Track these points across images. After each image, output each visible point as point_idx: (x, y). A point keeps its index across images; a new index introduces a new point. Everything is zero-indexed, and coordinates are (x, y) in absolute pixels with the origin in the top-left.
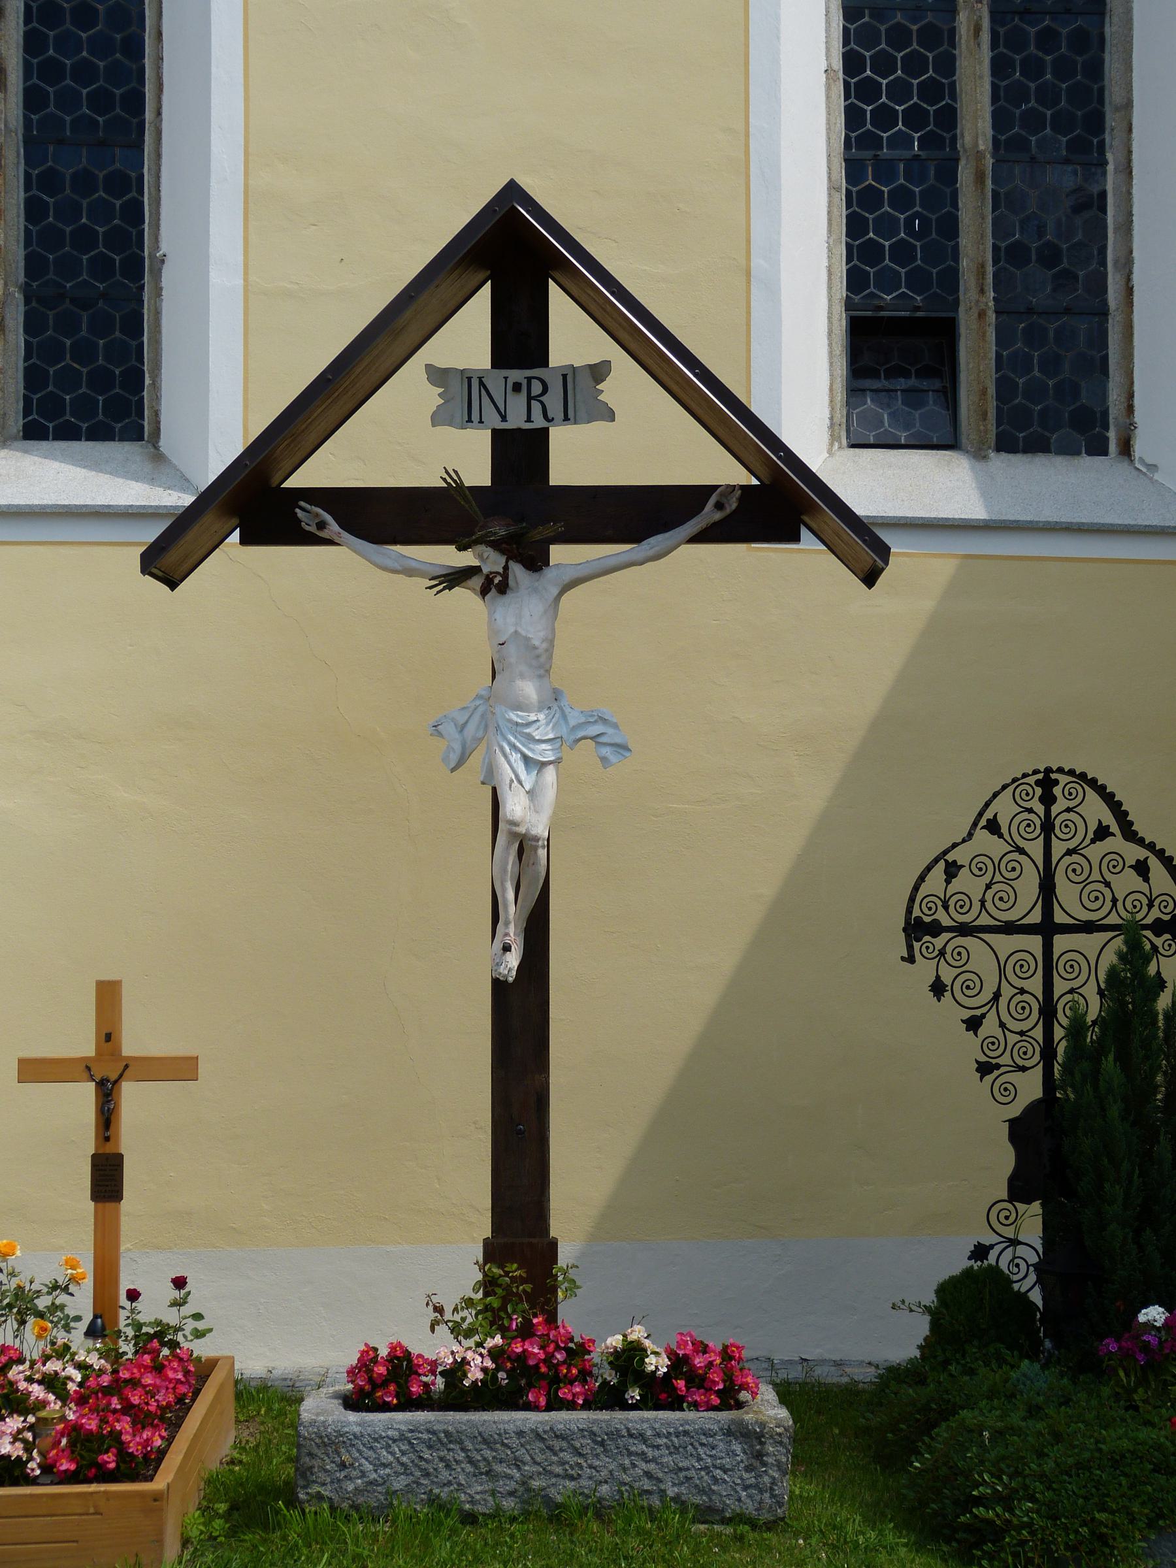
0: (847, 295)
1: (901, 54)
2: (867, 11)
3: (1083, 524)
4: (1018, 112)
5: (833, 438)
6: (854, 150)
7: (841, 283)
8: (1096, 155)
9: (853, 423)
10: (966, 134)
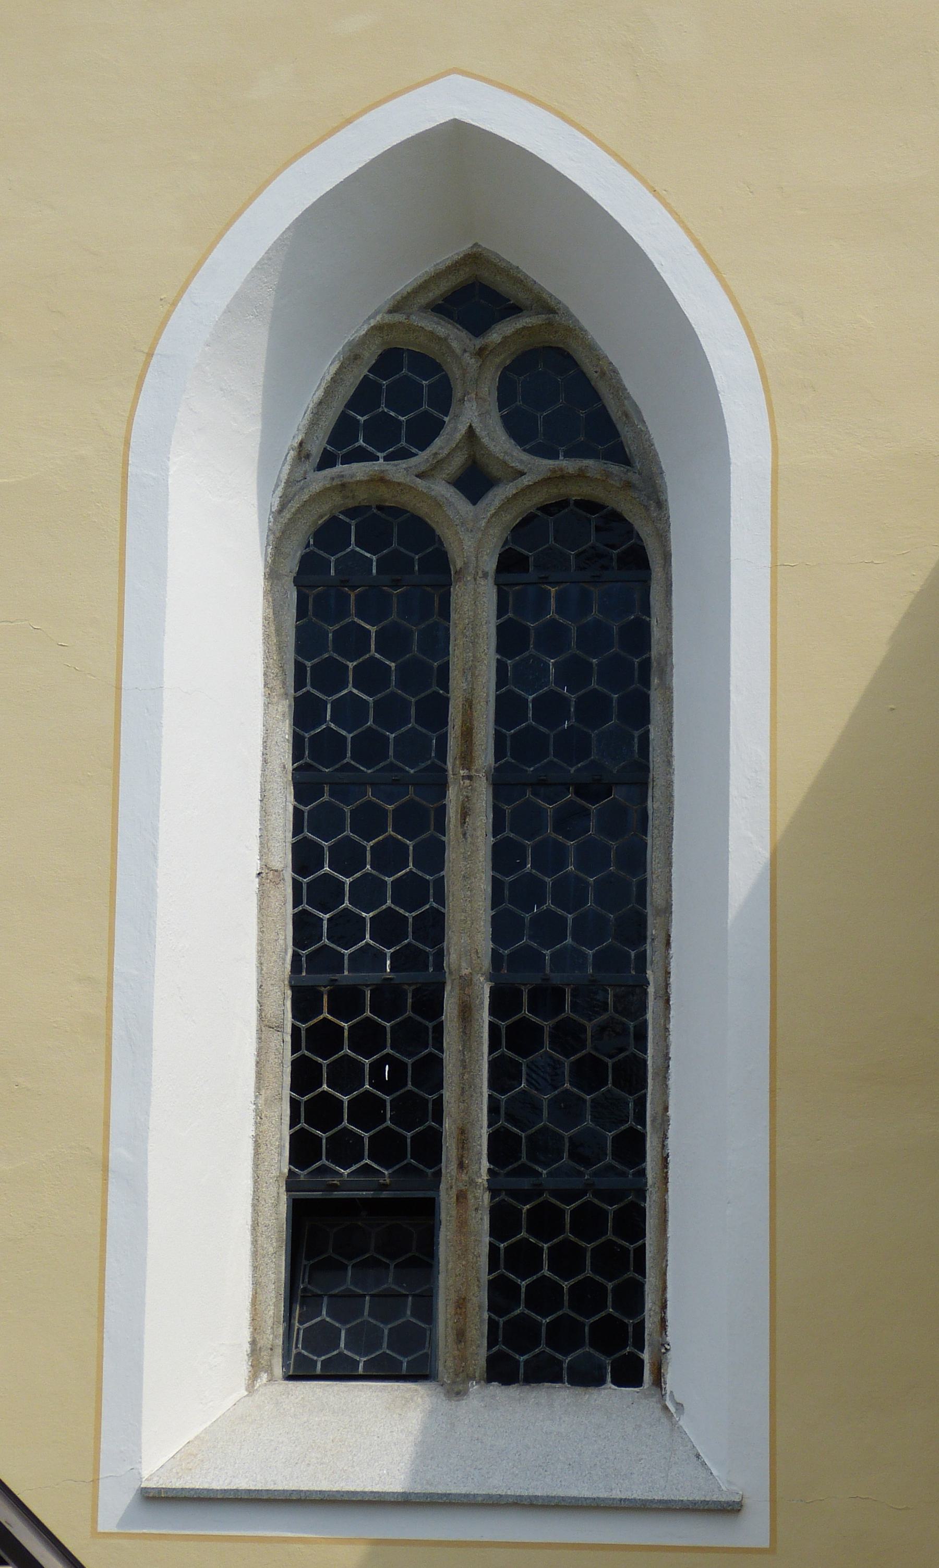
0: (290, 1170)
1: (371, 843)
2: (326, 788)
3: (536, 1497)
4: (528, 916)
5: (257, 1366)
6: (304, 974)
7: (280, 1154)
8: (633, 972)
9: (297, 1344)
10: (452, 951)
